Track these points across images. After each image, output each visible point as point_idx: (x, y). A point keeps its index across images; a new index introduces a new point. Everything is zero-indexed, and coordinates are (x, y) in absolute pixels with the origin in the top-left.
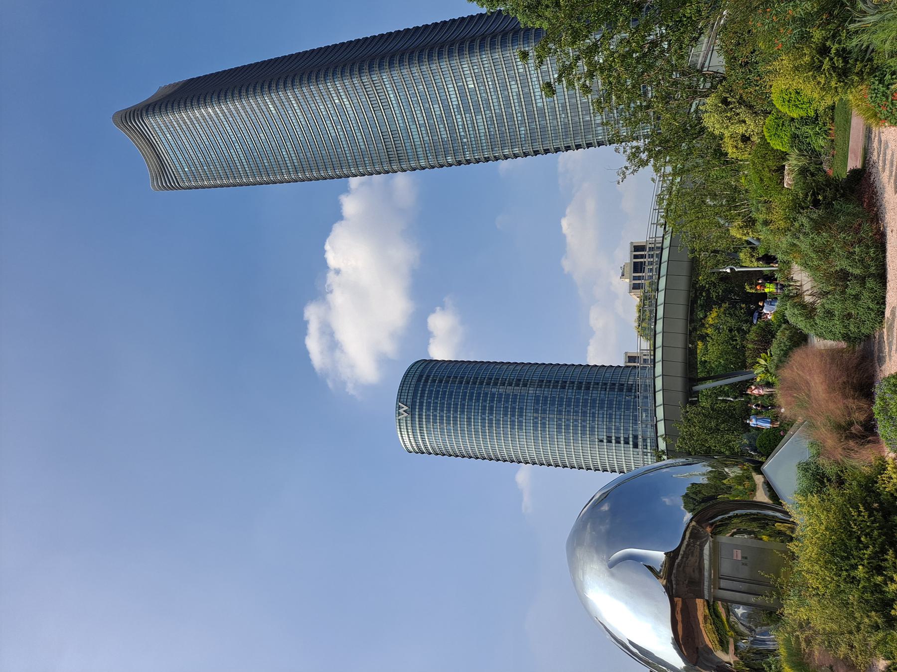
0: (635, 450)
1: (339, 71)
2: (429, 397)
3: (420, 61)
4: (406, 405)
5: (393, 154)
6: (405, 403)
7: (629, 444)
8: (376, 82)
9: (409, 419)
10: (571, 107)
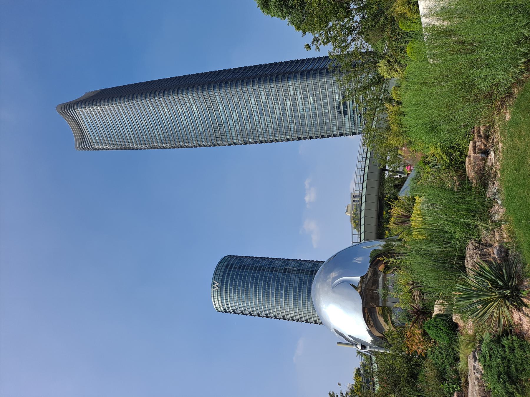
2: (232, 278)
3: (203, 90)
4: (218, 282)
6: (217, 281)
8: (279, 88)
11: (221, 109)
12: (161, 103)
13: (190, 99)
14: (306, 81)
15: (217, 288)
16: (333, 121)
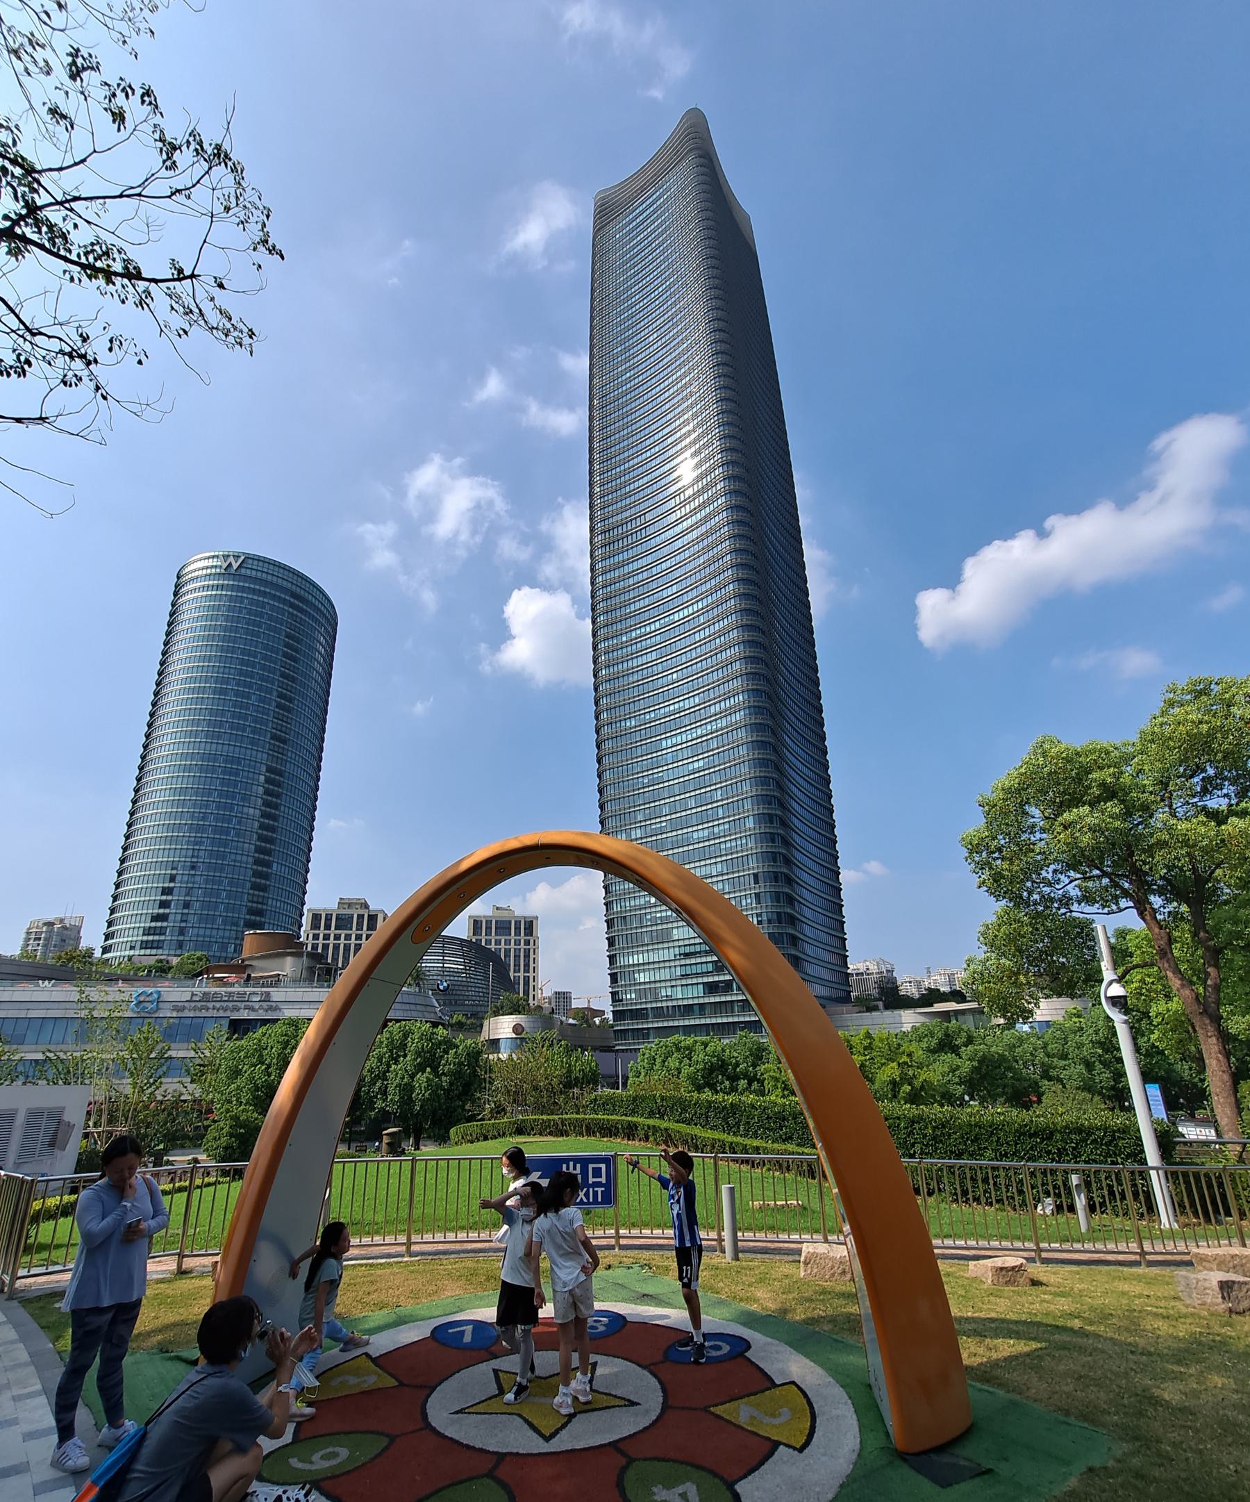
0: (149, 918)
1: (756, 636)
2: (252, 602)
3: (744, 627)
4: (240, 566)
5: (619, 698)
6: (245, 565)
7: (160, 908)
8: (742, 825)
9: (218, 570)
10: (664, 931)
11: (696, 765)
12: (711, 562)
13: (718, 640)
14: (754, 851)
15: (225, 565)
16: (638, 831)
